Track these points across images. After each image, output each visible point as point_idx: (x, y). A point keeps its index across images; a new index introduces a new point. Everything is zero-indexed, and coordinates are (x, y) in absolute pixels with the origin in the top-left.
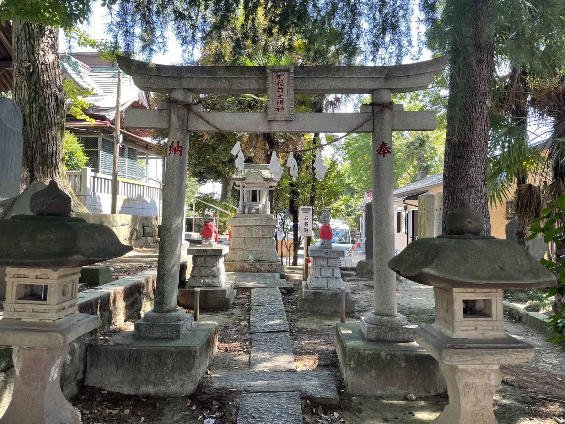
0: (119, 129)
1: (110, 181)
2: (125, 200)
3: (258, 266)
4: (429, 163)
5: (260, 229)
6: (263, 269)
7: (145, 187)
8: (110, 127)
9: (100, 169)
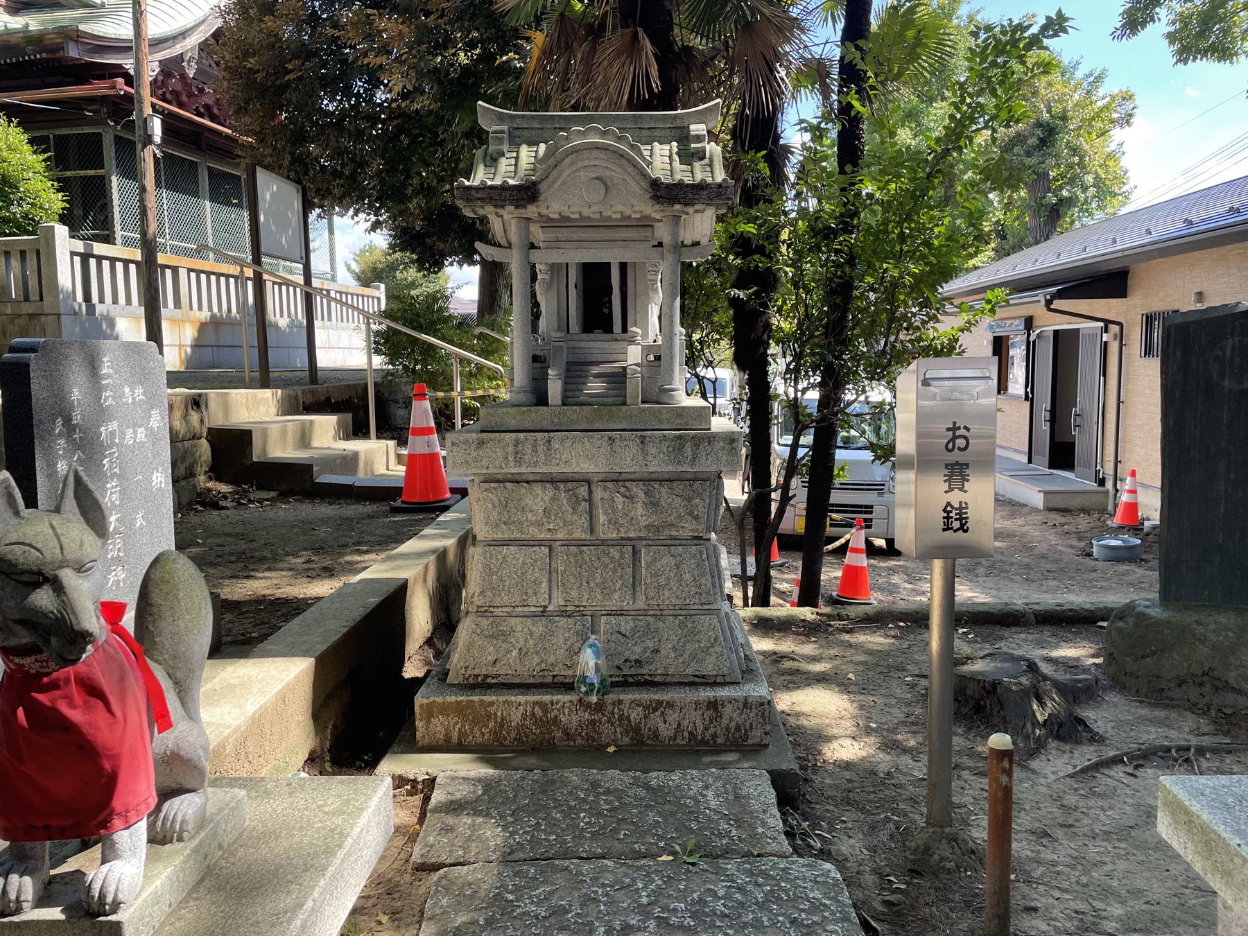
0: (148, 99)
1: (132, 267)
2: (203, 327)
3: (635, 714)
4: (1065, 193)
5: (638, 491)
6: (665, 731)
7: (183, 273)
8: (127, 94)
9: (119, 233)
